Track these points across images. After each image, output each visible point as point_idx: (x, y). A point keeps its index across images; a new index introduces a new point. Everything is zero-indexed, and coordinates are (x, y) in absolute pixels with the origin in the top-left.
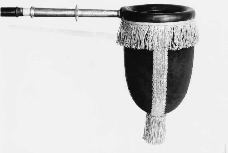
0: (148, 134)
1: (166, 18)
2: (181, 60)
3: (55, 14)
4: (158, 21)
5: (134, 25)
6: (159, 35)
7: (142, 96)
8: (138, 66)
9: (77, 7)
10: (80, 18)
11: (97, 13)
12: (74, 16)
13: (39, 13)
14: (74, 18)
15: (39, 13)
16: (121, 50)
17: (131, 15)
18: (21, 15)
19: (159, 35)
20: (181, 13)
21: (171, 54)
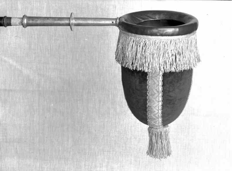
0: (156, 148)
1: (170, 30)
2: (178, 84)
3: (51, 23)
4: (155, 35)
5: (133, 38)
6: (158, 52)
7: (139, 108)
8: (134, 82)
9: (73, 15)
10: (75, 27)
11: (90, 22)
12: (69, 25)
13: (32, 22)
14: (69, 27)
15: (32, 22)
16: (119, 66)
17: (137, 24)
18: (9, 24)
19: (158, 52)
20: (180, 23)
21: (166, 76)
